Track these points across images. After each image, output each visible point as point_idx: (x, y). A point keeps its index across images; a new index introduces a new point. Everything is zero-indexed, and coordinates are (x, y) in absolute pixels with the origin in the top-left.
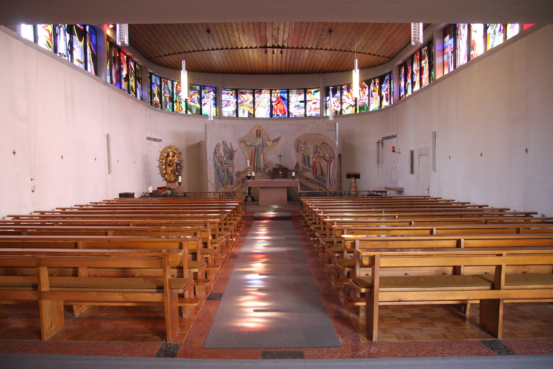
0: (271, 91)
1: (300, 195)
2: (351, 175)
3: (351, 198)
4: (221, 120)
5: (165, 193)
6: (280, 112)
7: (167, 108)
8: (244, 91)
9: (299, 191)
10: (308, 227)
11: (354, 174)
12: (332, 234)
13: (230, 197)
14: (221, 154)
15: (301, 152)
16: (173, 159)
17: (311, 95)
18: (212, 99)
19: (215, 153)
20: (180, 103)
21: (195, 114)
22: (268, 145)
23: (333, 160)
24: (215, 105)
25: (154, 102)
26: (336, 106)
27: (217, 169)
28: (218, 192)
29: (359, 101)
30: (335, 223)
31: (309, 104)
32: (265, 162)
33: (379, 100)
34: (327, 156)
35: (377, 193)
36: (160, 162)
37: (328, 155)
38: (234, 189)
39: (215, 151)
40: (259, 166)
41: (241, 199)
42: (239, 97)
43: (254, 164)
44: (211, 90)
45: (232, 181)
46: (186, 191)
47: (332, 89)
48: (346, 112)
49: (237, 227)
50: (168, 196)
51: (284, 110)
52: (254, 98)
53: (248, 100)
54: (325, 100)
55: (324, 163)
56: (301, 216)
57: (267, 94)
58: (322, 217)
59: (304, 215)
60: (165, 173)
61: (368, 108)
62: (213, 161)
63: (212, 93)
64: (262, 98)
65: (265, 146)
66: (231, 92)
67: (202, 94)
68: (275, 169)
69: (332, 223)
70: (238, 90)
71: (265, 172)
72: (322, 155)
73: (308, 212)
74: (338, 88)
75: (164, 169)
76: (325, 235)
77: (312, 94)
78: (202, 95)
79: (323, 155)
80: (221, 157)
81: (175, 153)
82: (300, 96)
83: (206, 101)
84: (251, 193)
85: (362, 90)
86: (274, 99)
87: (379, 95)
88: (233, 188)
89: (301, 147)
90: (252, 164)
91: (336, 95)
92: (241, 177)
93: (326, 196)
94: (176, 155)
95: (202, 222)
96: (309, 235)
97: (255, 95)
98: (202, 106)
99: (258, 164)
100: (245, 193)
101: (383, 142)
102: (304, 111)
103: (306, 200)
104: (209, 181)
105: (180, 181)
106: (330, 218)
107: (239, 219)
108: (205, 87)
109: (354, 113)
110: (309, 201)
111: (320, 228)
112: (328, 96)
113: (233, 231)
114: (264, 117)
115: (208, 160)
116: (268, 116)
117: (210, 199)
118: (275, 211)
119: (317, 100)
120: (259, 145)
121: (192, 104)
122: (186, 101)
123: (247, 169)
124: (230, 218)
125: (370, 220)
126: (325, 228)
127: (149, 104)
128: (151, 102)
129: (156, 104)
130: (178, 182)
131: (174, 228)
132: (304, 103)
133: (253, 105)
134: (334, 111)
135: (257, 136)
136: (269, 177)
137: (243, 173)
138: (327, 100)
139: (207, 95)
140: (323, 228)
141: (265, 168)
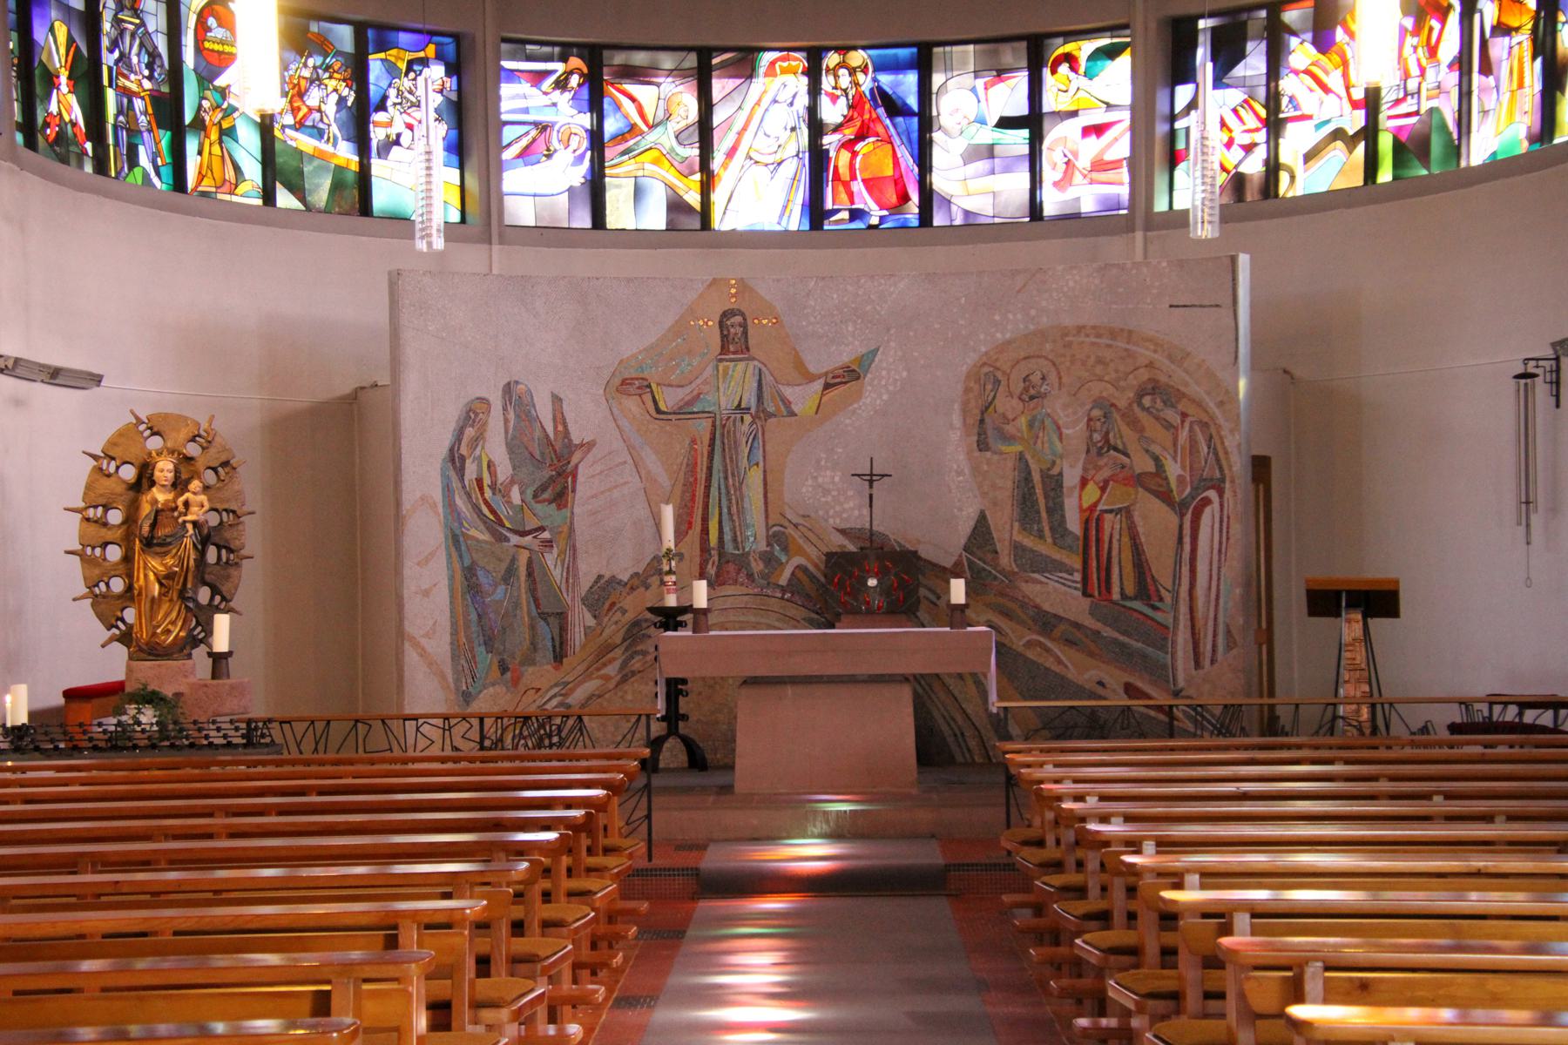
0: (814, 58)
1: (1000, 724)
2: (1338, 594)
3: (1340, 748)
4: (496, 248)
5: (119, 724)
6: (870, 193)
7: (137, 170)
8: (640, 58)
9: (995, 704)
10: (1057, 943)
11: (1353, 587)
12: (1221, 996)
13: (551, 746)
14: (490, 465)
15: (1004, 448)
16: (182, 499)
17: (1072, 75)
18: (436, 110)
19: (453, 460)
20: (228, 133)
21: (326, 211)
22: (795, 408)
23: (1212, 494)
24: (459, 149)
25: (47, 125)
26: (1235, 147)
27: (467, 562)
28: (469, 710)
29: (1398, 102)
30: (1242, 921)
31: (1059, 137)
32: (774, 518)
33: (1538, 87)
34: (1173, 470)
35: (1520, 714)
36: (88, 520)
37: (1183, 468)
38: (572, 690)
39: (451, 450)
40: (735, 540)
41: (619, 757)
42: (606, 101)
43: (705, 531)
44: (431, 50)
45: (563, 643)
46: (259, 711)
47: (1213, 29)
48: (1302, 182)
49: (594, 946)
50: (135, 747)
51: (899, 182)
52: (706, 106)
53: (668, 116)
54: (1162, 107)
55: (1155, 519)
56: (1011, 867)
57: (789, 79)
58: (1148, 880)
59: (1028, 858)
60: (120, 596)
61: (1455, 150)
62: (441, 510)
63: (437, 71)
64: (758, 103)
65: (771, 415)
66: (560, 67)
67: (372, 78)
68: (837, 562)
69: (1222, 918)
70: (606, 53)
71: (772, 580)
72: (1144, 464)
73: (1058, 842)
74: (1250, 22)
75: (117, 564)
76: (1176, 996)
77: (1082, 70)
78: (372, 87)
79: (1150, 467)
80: (493, 487)
81: (189, 459)
82: (1001, 88)
83: (398, 126)
84: (685, 717)
85: (1416, 31)
86: (831, 112)
87: (1534, 58)
88: (567, 688)
89: (1004, 416)
90: (690, 527)
91: (1239, 71)
92: (619, 614)
93: (1172, 736)
94: (195, 475)
95: (364, 921)
96: (1061, 997)
97: (714, 81)
98: (369, 158)
99: (727, 529)
100: (644, 719)
101: (1558, 370)
102: (1027, 185)
103: (1041, 765)
104: (412, 639)
105: (221, 642)
106: (1203, 887)
107: (605, 889)
108: (392, 35)
109: (1361, 183)
110: (1057, 765)
111: (1134, 951)
112: (1184, 81)
113: (567, 975)
114: (767, 228)
115: (407, 505)
116: (795, 221)
117: (415, 760)
118: (835, 835)
119: (1109, 106)
120: (739, 407)
121: (305, 142)
122: (266, 127)
123: (657, 560)
124: (546, 884)
125: (1475, 900)
126: (1168, 954)
127: (13, 139)
128: (29, 128)
129: (61, 138)
130: (211, 654)
131: (166, 965)
132: (1025, 133)
133: (701, 148)
134: (1225, 175)
135: (724, 349)
136: (800, 613)
137: (632, 589)
138: (1179, 107)
139: (406, 83)
140: (1157, 951)
141: (772, 553)
